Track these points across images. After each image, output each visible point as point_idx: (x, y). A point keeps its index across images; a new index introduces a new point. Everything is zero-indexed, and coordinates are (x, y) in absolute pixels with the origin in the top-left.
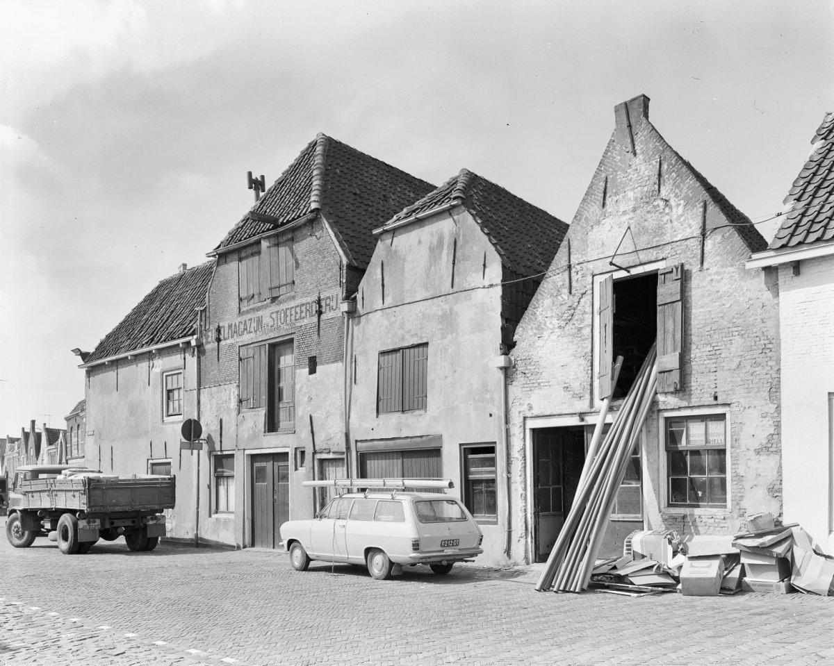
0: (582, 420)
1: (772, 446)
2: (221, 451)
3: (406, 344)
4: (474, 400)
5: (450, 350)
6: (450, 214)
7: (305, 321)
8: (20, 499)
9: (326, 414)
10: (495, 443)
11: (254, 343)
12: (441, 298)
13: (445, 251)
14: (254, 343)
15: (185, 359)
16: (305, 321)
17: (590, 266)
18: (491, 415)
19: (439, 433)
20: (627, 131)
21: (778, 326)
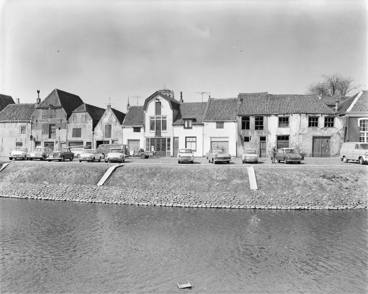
10: (290, 135)
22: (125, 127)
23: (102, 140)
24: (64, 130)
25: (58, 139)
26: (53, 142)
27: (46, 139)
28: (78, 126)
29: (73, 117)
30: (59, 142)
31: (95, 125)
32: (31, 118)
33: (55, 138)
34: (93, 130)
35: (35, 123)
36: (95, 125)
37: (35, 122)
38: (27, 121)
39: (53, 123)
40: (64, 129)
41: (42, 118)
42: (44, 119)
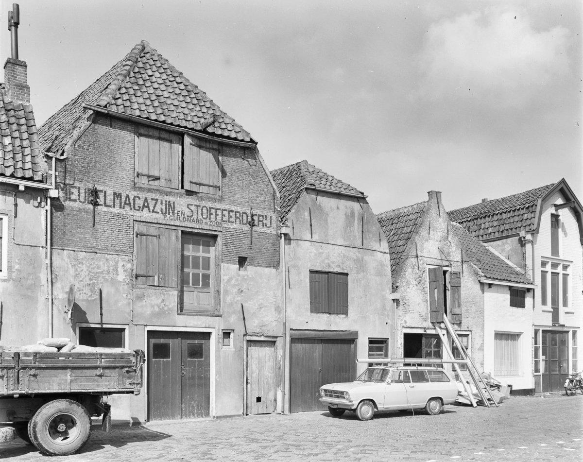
0: (425, 331)
1: (481, 349)
2: (101, 323)
3: (332, 270)
4: (378, 314)
5: (363, 282)
6: (318, 193)
7: (234, 226)
8: (80, 327)
9: (259, 305)
10: (388, 339)
11: (159, 224)
12: (355, 249)
13: (356, 222)
14: (159, 224)
15: (16, 205)
16: (234, 226)
17: (425, 259)
18: (387, 323)
19: (357, 330)
20: (437, 205)
21: (484, 304)
22: (490, 285)
23: (421, 331)
25: (233, 321)
26: (207, 336)
27: (161, 313)
28: (333, 259)
29: (307, 214)
30: (240, 330)
31: (397, 267)
35: (77, 205)
36: (397, 267)
37: (76, 204)
39: (205, 226)
41: (135, 187)
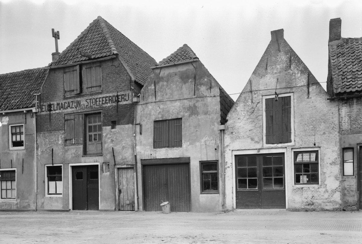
23: (255, 152)
24: (127, 126)
32: (36, 102)
33: (101, 155)
34: (224, 121)
38: (25, 110)
40: (128, 124)
41: (65, 98)
42: (70, 100)
